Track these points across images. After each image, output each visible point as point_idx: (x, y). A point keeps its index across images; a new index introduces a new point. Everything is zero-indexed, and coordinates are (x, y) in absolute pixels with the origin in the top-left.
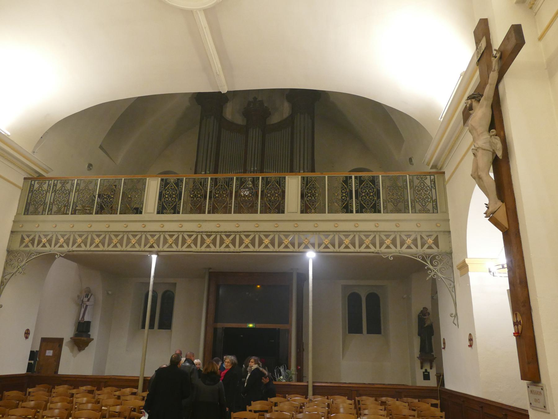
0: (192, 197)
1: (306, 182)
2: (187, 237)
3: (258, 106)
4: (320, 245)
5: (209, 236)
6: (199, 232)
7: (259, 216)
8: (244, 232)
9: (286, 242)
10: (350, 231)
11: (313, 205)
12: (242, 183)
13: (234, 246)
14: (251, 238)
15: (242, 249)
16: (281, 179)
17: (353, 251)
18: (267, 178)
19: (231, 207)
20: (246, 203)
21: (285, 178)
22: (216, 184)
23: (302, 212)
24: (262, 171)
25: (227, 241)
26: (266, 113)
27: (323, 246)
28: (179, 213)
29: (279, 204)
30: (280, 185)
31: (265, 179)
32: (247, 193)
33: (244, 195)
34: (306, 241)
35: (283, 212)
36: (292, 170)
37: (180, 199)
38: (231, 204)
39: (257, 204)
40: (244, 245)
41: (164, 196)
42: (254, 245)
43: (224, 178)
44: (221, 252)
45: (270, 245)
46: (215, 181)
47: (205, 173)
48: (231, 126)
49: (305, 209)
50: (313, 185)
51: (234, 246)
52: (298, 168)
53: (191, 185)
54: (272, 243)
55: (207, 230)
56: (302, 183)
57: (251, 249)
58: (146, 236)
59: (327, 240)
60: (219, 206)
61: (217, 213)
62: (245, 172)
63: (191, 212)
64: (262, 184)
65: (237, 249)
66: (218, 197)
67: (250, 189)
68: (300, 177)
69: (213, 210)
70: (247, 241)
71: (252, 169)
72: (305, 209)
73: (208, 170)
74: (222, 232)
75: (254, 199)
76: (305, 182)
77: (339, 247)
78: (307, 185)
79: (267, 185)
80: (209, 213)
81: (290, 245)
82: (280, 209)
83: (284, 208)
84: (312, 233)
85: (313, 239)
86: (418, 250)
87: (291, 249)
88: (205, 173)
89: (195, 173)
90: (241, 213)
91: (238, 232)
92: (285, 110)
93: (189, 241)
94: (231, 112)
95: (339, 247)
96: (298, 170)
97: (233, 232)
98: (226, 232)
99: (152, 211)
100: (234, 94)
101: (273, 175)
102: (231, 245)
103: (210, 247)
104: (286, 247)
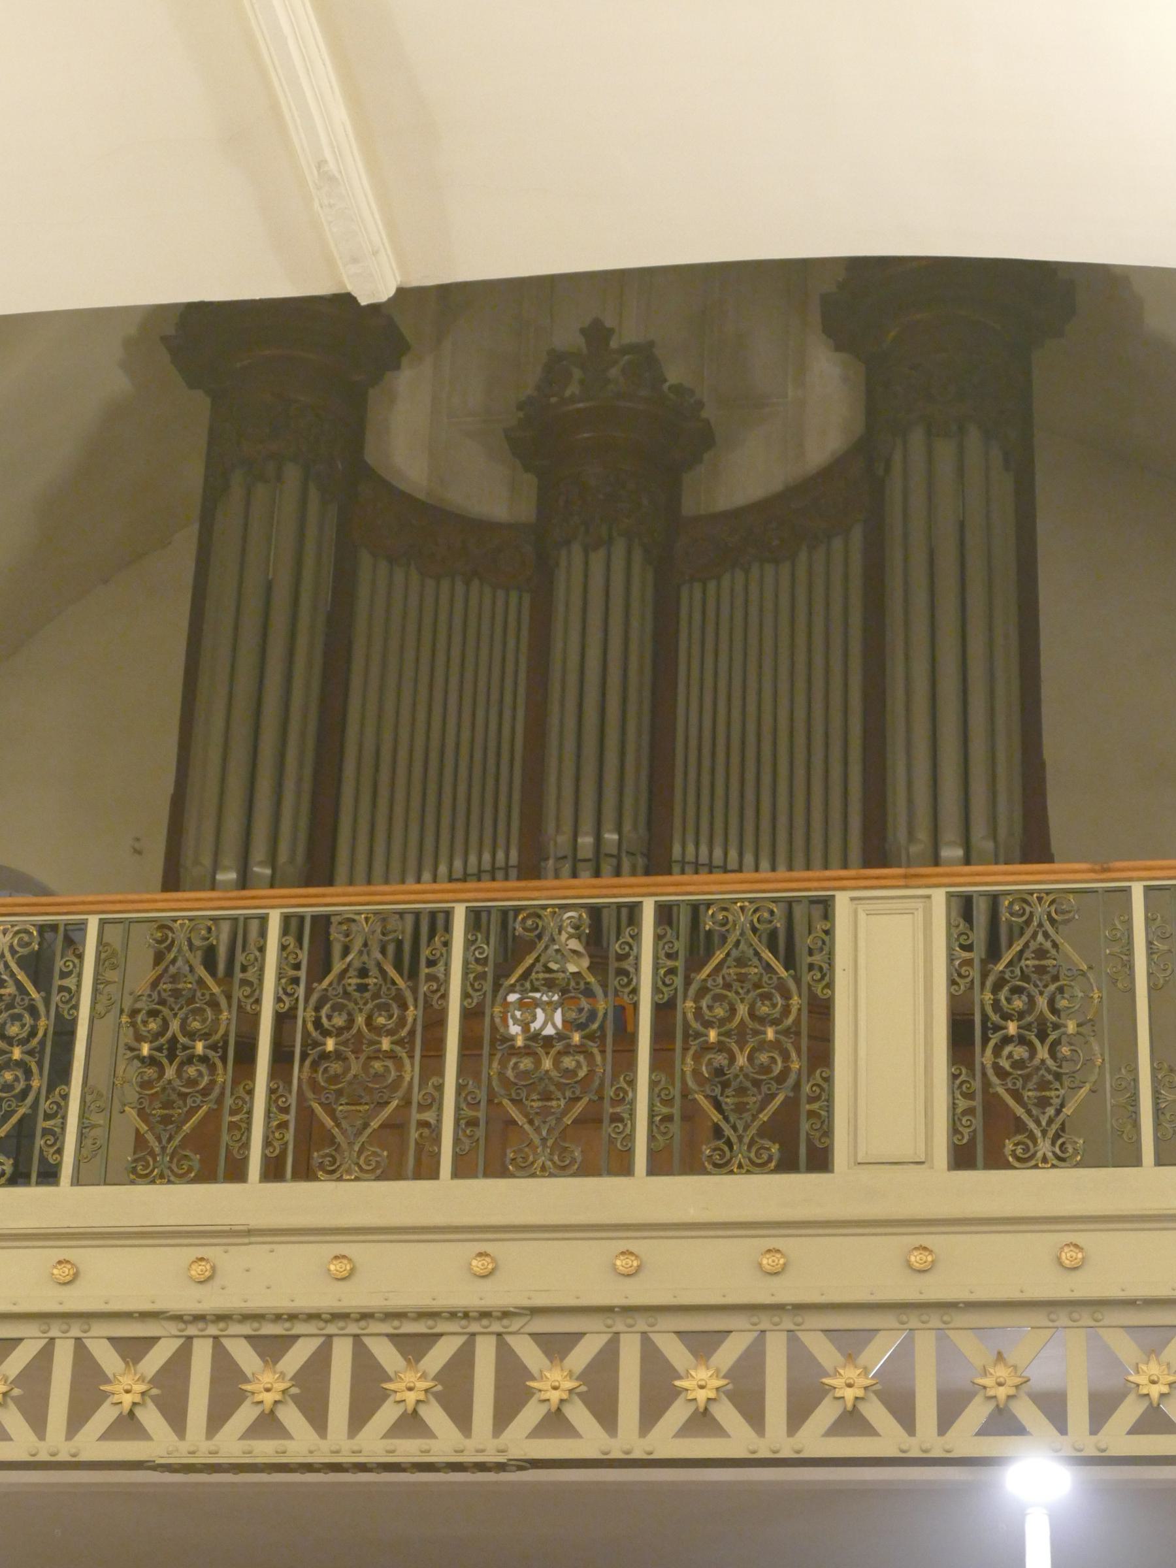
0: (152, 1061)
1: (986, 937)
2: (108, 1359)
3: (612, 387)
4: (1102, 1407)
5: (413, 1347)
6: (199, 1318)
7: (642, 1194)
8: (535, 1311)
9: (849, 1382)
10: (293, 1317)
11: (1043, 1103)
12: (510, 947)
13: (462, 1418)
14: (581, 1356)
15: (519, 1441)
16: (799, 911)
17: (891, 1452)
18: (696, 909)
19: (433, 1131)
20: (547, 1097)
21: (826, 906)
22: (321, 965)
23: (962, 1158)
24: (656, 861)
25: (410, 1383)
26: (678, 437)
27: (1129, 1411)
28: (49, 1176)
29: (792, 1104)
30: (790, 962)
31: (684, 919)
32: (549, 1021)
33: (535, 1037)
34: (998, 1381)
35: (820, 1161)
36: (877, 853)
37: (61, 1074)
38: (434, 1102)
39: (624, 1099)
40: (531, 1414)
41: (407, 1042)
42: (607, 1416)
43: (383, 917)
44: (362, 1467)
45: (726, 1413)
46: (316, 938)
47: (244, 882)
48: (433, 535)
49: (986, 1136)
50: (1041, 953)
51: (462, 1418)
52: (923, 835)
53: (140, 974)
54: (746, 1394)
55: (398, 1302)
56: (959, 943)
57: (590, 1440)
58: (81, 1350)
59: (1154, 1369)
60: (343, 1126)
61: (333, 1172)
62: (531, 868)
63: (144, 1169)
64: (663, 953)
65: (482, 1442)
66: (338, 1055)
67: (570, 990)
68: (939, 897)
69: (304, 1155)
70: (554, 1381)
71: (586, 840)
72: (986, 1136)
73: (259, 851)
74: (366, 1316)
75: (604, 1064)
76: (979, 936)
77: (944, 1425)
78: (993, 953)
79: (695, 961)
80: (273, 1171)
81: (875, 1412)
82: (800, 1145)
83: (828, 1133)
84: (1040, 1318)
85: (1059, 1359)
86: (470, 1444)
87: (889, 1438)
88: (244, 882)
89: (172, 881)
90: (504, 1173)
91: (485, 1314)
92: (816, 407)
93: (127, 1385)
94: (424, 436)
95: (944, 1425)
96: (919, 847)
97: (453, 1315)
98: (400, 1315)
99: (906, 1149)
100: (448, 305)
101: (737, 891)
102: (434, 1416)
103: (281, 1432)
104: (852, 1421)
